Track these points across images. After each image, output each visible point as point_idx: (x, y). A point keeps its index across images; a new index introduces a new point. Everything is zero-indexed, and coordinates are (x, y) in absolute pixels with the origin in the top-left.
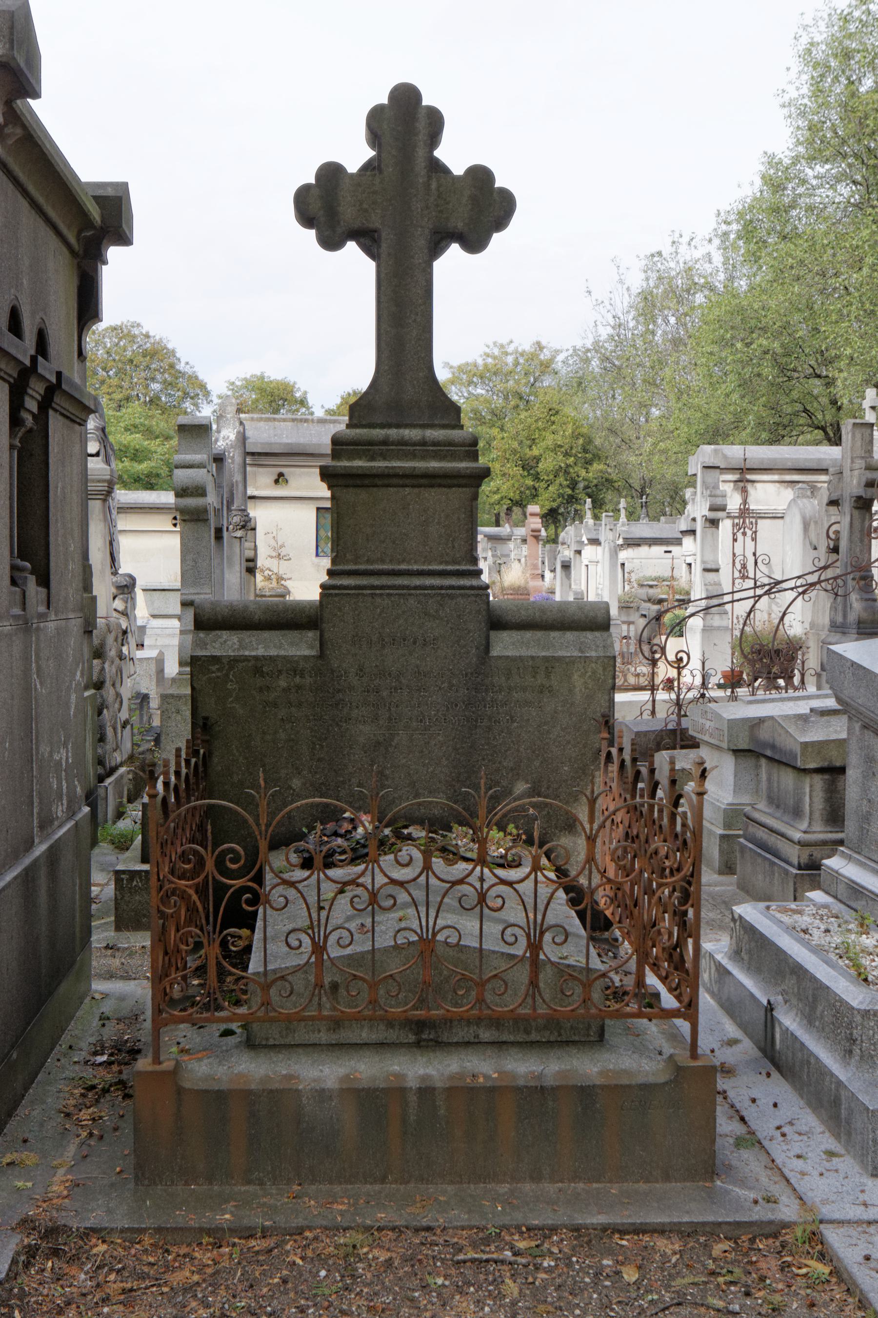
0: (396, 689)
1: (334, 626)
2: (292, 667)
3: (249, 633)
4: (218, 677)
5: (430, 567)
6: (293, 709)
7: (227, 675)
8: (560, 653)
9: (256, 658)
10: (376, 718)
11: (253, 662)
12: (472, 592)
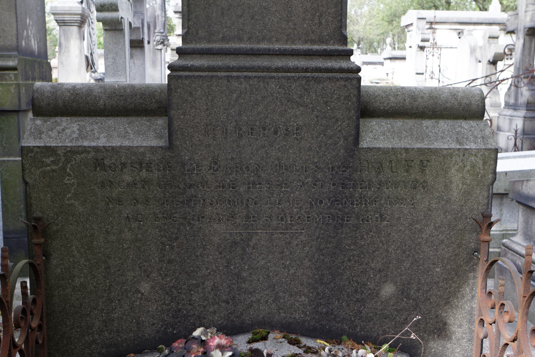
0: (254, 183)
1: (184, 114)
2: (137, 159)
3: (92, 119)
4: (53, 171)
5: (294, 47)
6: (139, 206)
7: (64, 168)
8: (437, 145)
9: (96, 149)
10: (233, 216)
11: (93, 154)
12: (342, 75)
